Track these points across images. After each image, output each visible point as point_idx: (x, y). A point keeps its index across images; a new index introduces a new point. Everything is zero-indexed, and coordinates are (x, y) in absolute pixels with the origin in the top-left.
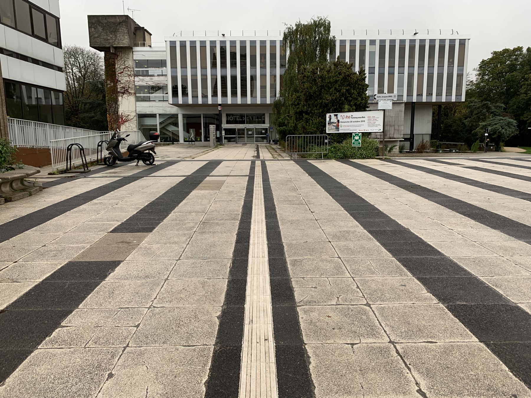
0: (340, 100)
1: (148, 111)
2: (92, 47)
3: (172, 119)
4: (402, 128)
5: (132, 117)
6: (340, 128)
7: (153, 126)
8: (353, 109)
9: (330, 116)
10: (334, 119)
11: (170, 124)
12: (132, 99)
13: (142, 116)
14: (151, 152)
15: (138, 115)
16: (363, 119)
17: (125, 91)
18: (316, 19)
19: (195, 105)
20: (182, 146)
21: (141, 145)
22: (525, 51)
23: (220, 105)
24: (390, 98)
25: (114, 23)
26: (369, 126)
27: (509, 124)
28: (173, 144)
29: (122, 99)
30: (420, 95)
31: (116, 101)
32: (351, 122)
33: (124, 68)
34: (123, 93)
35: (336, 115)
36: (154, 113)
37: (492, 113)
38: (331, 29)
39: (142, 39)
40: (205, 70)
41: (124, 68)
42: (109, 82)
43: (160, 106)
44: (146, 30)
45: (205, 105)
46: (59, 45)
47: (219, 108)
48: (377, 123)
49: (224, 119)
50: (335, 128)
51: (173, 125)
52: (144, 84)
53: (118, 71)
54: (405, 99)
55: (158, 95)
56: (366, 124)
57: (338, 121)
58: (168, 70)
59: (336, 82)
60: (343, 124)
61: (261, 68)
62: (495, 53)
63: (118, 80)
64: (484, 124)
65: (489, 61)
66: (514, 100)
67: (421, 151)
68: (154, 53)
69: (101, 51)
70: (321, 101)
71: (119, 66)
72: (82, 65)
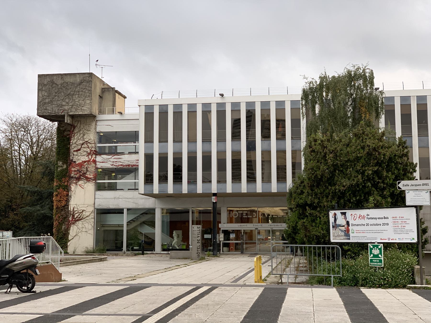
0: (364, 187)
1: (112, 205)
2: (40, 116)
3: (146, 216)
5: (88, 214)
6: (351, 235)
8: (387, 202)
9: (335, 214)
10: (341, 220)
11: (144, 223)
12: (90, 186)
13: (103, 213)
14: (30, 271)
15: (97, 209)
17: (81, 175)
20: (242, 229)
23: (215, 195)
24: (425, 187)
25: (73, 84)
28: (143, 254)
29: (76, 188)
31: (67, 189)
32: (368, 225)
33: (83, 144)
34: (78, 179)
35: (344, 214)
36: (121, 207)
39: (111, 104)
41: (83, 144)
42: (60, 163)
43: (129, 197)
44: (117, 92)
45: (192, 195)
47: (214, 199)
48: (407, 227)
49: (224, 216)
50: (343, 234)
51: (148, 225)
53: (73, 147)
55: (128, 180)
56: (390, 228)
57: (348, 223)
58: (141, 143)
59: (358, 159)
60: (355, 228)
63: (72, 161)
70: (333, 188)
71: (75, 141)
72: (34, 140)
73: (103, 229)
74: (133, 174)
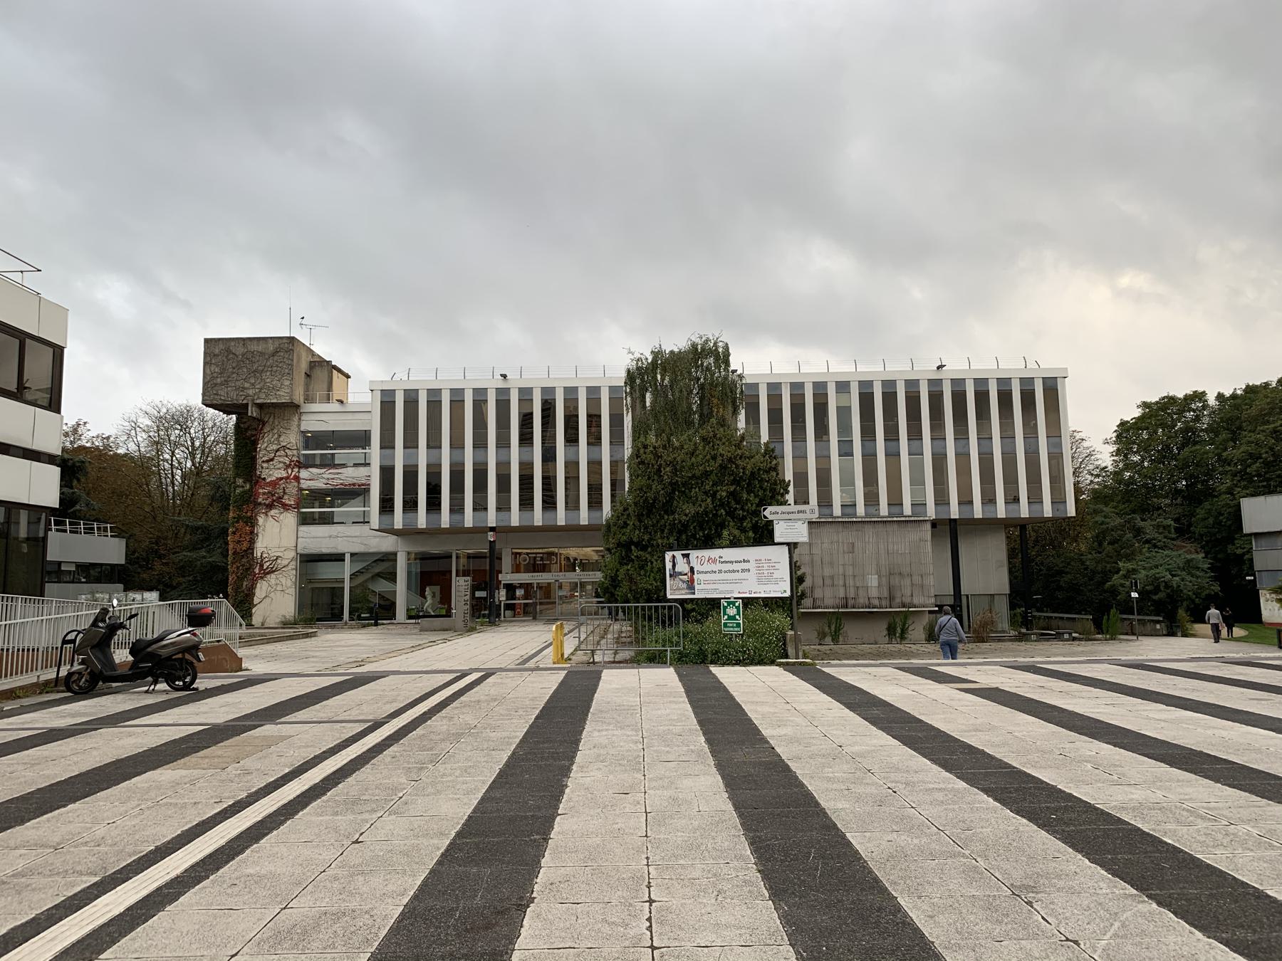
0: (715, 515)
1: (326, 547)
2: (207, 405)
3: (382, 565)
4: (930, 581)
5: (285, 562)
6: (697, 587)
7: (337, 581)
8: (748, 538)
10: (682, 566)
11: (379, 575)
12: (290, 519)
13: (309, 560)
14: (188, 656)
16: (745, 566)
18: (698, 341)
19: (433, 532)
21: (162, 639)
22: (1212, 400)
23: (492, 529)
25: (262, 354)
26: (760, 582)
27: (1189, 566)
28: (376, 624)
29: (265, 521)
30: (966, 501)
31: (252, 522)
32: (720, 571)
33: (278, 450)
34: (270, 506)
35: (686, 556)
36: (340, 550)
37: (1148, 542)
38: (731, 358)
40: (941, 442)
41: (278, 450)
43: (354, 535)
44: (335, 367)
45: (457, 531)
46: (54, 404)
47: (491, 536)
49: (507, 562)
50: (685, 586)
52: (319, 484)
53: (262, 456)
54: (931, 512)
55: (353, 508)
56: (752, 576)
57: (692, 569)
59: (706, 474)
60: (702, 577)
61: (589, 444)
62: (1145, 405)
64: (1129, 566)
65: (1135, 423)
66: (1207, 505)
67: (982, 635)
68: (350, 416)
69: (228, 413)
70: (671, 518)
71: (266, 446)
73: (310, 586)
74: (361, 498)
